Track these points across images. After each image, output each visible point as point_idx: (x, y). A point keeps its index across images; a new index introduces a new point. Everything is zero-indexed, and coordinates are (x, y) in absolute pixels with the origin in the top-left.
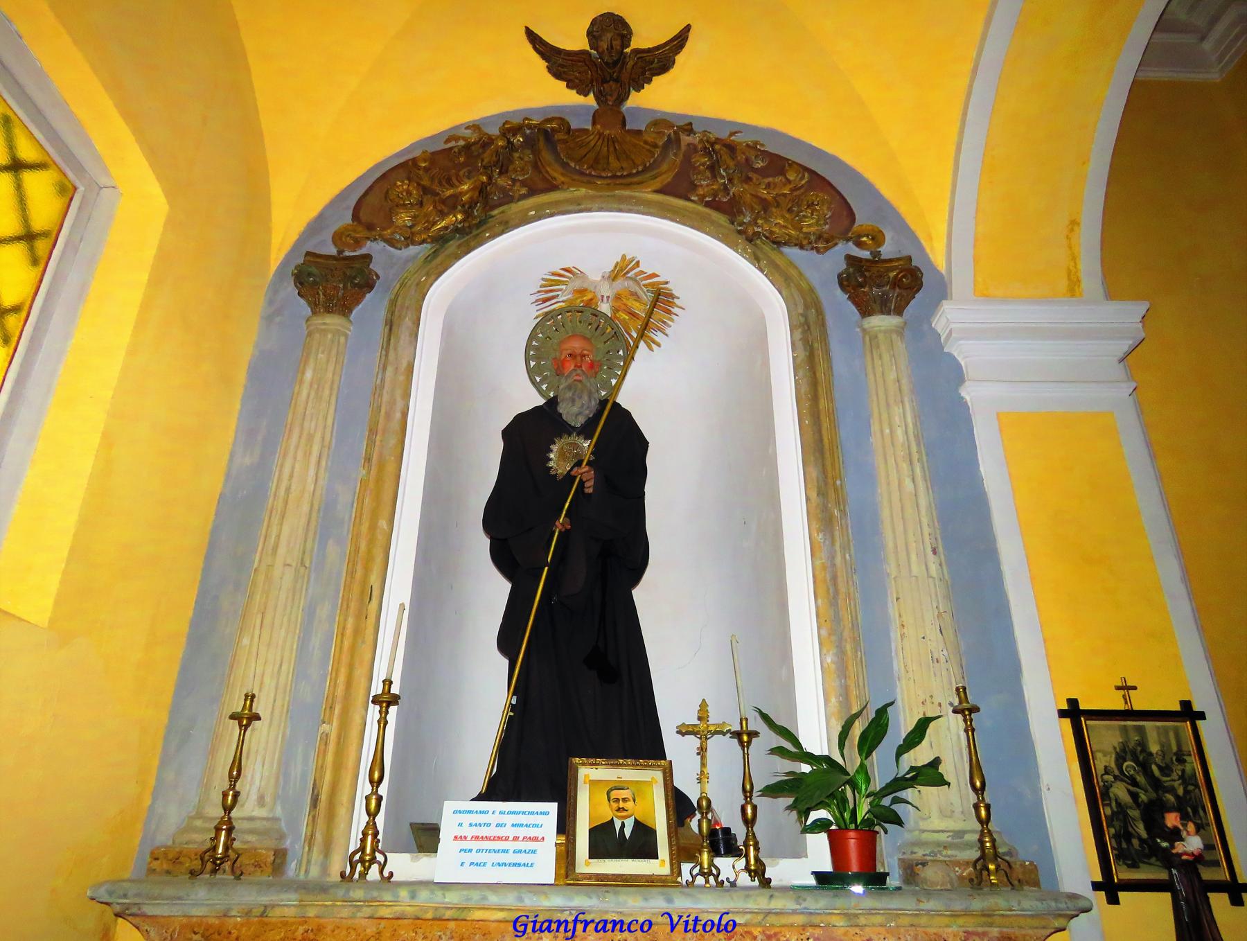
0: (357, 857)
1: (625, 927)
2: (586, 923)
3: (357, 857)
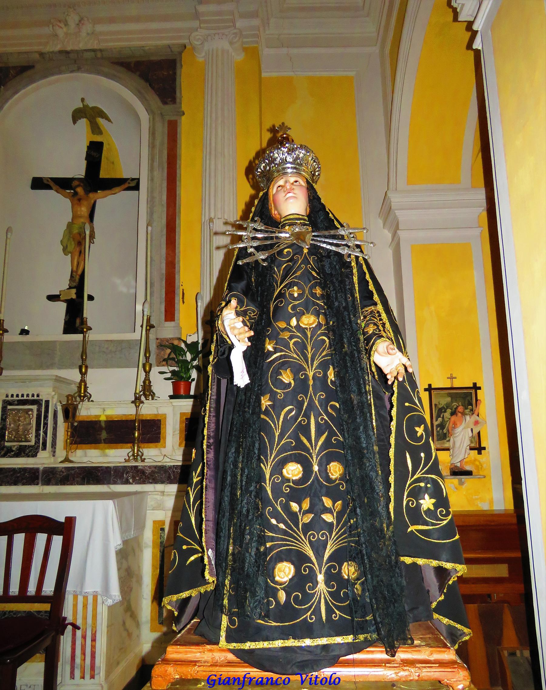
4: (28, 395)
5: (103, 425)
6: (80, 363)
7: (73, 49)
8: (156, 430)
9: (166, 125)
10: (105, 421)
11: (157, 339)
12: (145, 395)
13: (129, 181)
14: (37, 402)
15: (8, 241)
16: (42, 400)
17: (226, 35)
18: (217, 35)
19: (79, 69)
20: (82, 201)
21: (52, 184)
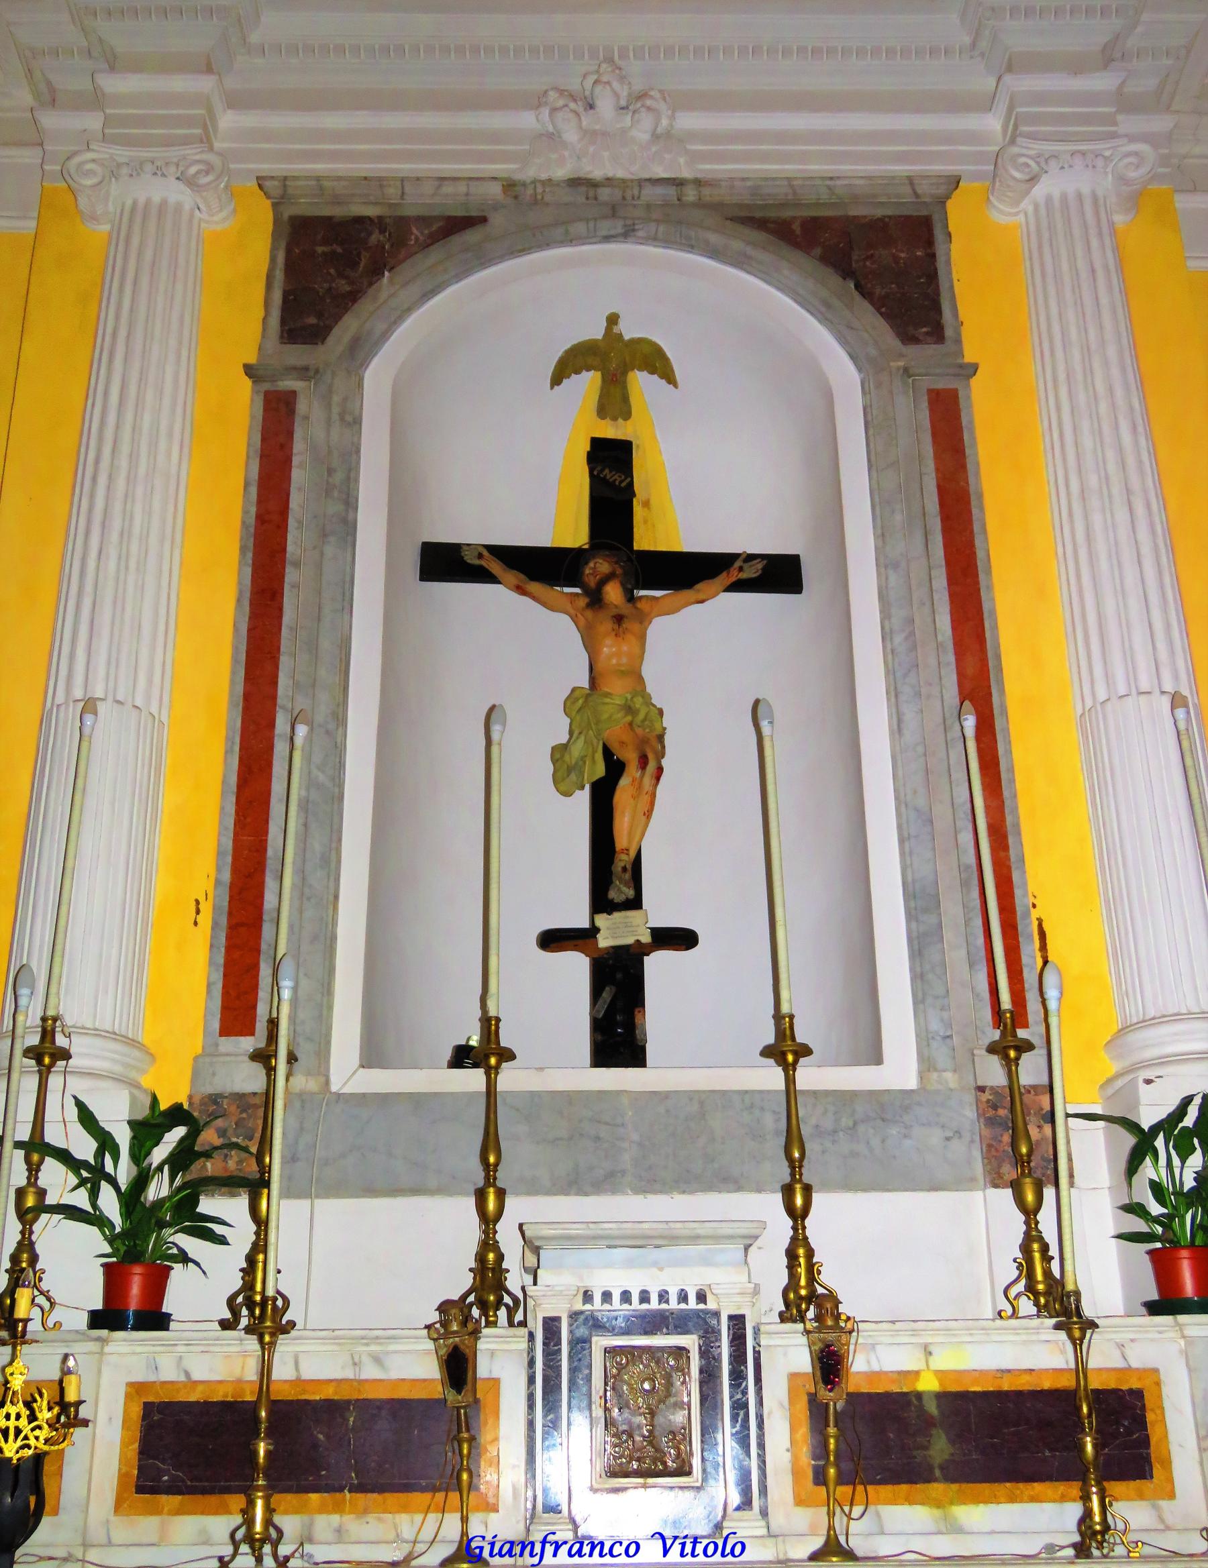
0: (240, 1299)
1: (606, 1550)
2: (557, 1547)
3: (239, 1535)
4: (683, 1297)
5: (932, 1408)
6: (785, 1175)
7: (610, 175)
8: (1129, 1432)
9: (925, 405)
10: (941, 1396)
11: (981, 1089)
12: (483, 1305)
13: (738, 564)
14: (703, 1324)
15: (495, 749)
16: (717, 1314)
17: (1106, 158)
18: (1053, 163)
19: (627, 234)
20: (626, 624)
21: (495, 567)
